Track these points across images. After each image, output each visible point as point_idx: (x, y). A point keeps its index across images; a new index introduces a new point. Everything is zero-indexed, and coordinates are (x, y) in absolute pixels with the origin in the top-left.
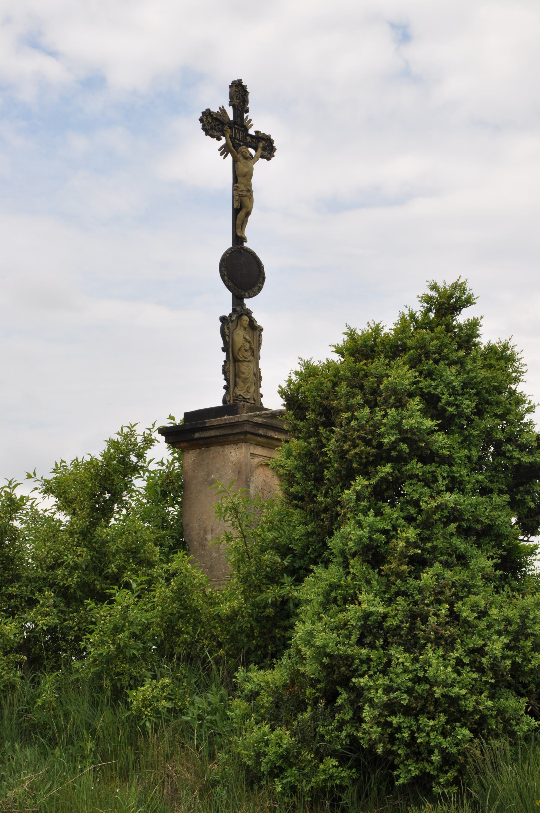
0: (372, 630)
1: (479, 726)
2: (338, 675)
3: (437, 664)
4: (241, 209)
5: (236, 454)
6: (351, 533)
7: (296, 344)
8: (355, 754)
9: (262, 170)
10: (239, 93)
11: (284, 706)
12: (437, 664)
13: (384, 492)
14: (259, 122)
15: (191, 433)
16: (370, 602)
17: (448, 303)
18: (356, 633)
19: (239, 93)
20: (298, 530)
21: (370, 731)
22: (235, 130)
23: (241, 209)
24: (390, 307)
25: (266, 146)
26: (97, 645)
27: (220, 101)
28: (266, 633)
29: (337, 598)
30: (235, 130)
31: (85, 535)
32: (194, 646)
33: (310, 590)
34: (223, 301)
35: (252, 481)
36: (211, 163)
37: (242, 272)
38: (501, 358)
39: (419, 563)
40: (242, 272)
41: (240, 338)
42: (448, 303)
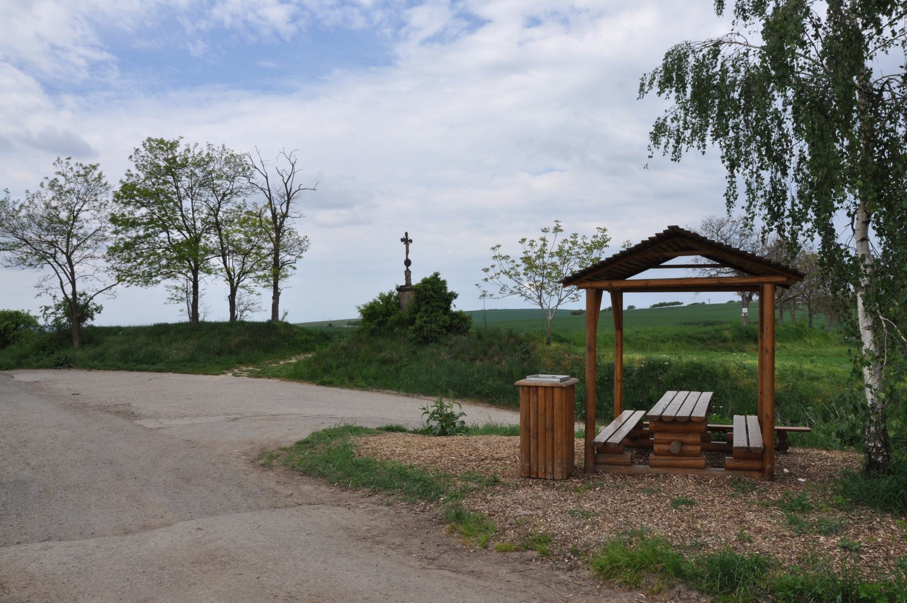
0: (425, 322)
1: (439, 333)
2: (421, 328)
3: (434, 326)
4: (407, 252)
5: (407, 293)
6: (423, 309)
7: (416, 280)
8: (423, 337)
9: (411, 245)
10: (406, 234)
11: (415, 331)
12: (434, 326)
13: (428, 303)
14: (410, 238)
15: (400, 289)
16: (425, 318)
17: (436, 275)
18: (409, 296)
19: (406, 234)
20: (416, 307)
21: (425, 334)
22: (406, 241)
23: (407, 252)
24: (428, 275)
25: (411, 241)
26: (389, 323)
27: (403, 236)
28: (412, 321)
29: (421, 317)
30: (406, 241)
31: (386, 307)
32: (401, 323)
33: (418, 316)
34: (405, 268)
35: (408, 300)
36: (404, 246)
37: (408, 263)
38: (444, 282)
39: (432, 313)
40: (408, 263)
41: (408, 274)
42: (436, 275)
